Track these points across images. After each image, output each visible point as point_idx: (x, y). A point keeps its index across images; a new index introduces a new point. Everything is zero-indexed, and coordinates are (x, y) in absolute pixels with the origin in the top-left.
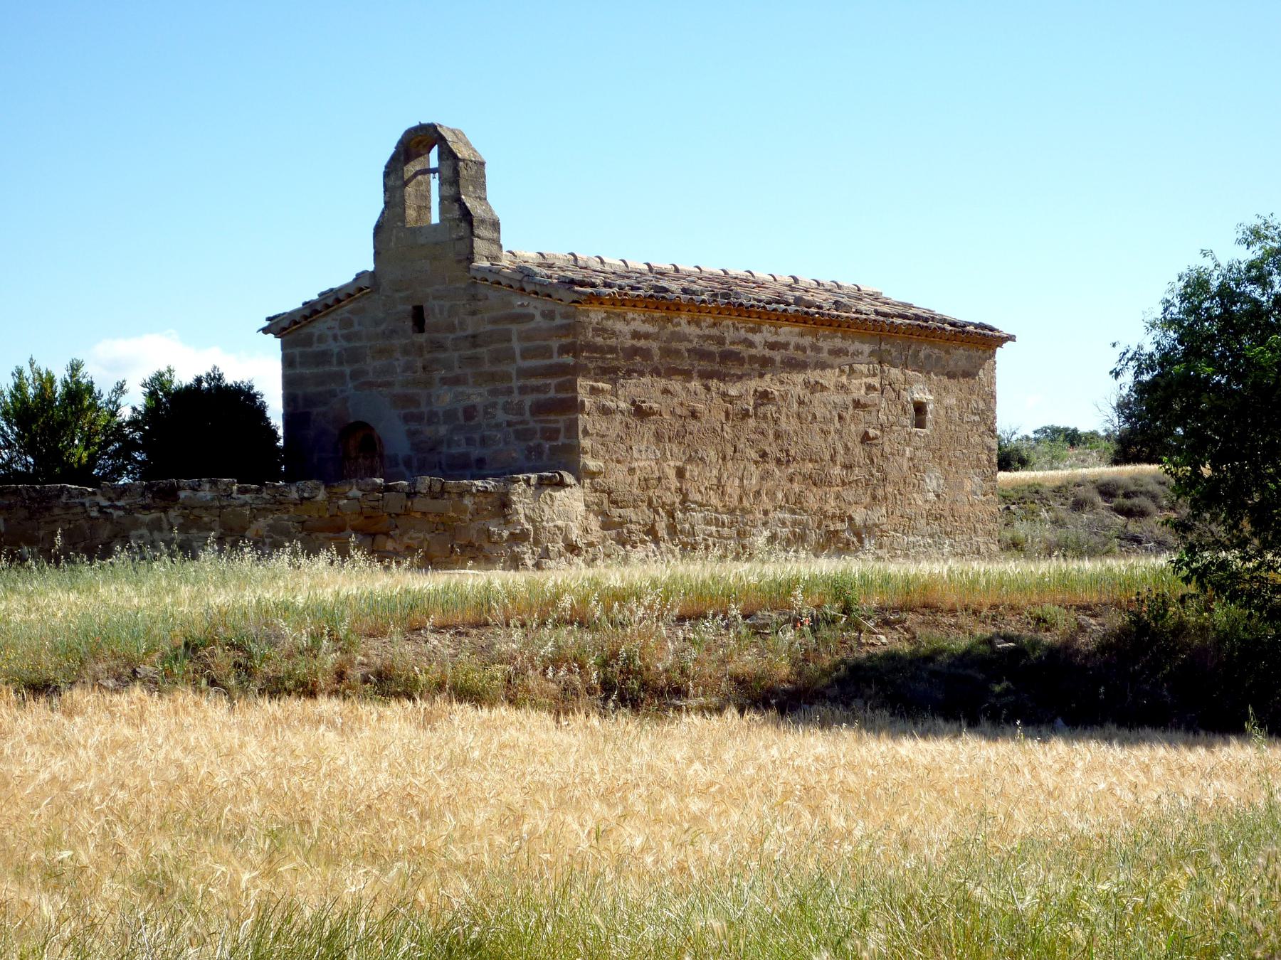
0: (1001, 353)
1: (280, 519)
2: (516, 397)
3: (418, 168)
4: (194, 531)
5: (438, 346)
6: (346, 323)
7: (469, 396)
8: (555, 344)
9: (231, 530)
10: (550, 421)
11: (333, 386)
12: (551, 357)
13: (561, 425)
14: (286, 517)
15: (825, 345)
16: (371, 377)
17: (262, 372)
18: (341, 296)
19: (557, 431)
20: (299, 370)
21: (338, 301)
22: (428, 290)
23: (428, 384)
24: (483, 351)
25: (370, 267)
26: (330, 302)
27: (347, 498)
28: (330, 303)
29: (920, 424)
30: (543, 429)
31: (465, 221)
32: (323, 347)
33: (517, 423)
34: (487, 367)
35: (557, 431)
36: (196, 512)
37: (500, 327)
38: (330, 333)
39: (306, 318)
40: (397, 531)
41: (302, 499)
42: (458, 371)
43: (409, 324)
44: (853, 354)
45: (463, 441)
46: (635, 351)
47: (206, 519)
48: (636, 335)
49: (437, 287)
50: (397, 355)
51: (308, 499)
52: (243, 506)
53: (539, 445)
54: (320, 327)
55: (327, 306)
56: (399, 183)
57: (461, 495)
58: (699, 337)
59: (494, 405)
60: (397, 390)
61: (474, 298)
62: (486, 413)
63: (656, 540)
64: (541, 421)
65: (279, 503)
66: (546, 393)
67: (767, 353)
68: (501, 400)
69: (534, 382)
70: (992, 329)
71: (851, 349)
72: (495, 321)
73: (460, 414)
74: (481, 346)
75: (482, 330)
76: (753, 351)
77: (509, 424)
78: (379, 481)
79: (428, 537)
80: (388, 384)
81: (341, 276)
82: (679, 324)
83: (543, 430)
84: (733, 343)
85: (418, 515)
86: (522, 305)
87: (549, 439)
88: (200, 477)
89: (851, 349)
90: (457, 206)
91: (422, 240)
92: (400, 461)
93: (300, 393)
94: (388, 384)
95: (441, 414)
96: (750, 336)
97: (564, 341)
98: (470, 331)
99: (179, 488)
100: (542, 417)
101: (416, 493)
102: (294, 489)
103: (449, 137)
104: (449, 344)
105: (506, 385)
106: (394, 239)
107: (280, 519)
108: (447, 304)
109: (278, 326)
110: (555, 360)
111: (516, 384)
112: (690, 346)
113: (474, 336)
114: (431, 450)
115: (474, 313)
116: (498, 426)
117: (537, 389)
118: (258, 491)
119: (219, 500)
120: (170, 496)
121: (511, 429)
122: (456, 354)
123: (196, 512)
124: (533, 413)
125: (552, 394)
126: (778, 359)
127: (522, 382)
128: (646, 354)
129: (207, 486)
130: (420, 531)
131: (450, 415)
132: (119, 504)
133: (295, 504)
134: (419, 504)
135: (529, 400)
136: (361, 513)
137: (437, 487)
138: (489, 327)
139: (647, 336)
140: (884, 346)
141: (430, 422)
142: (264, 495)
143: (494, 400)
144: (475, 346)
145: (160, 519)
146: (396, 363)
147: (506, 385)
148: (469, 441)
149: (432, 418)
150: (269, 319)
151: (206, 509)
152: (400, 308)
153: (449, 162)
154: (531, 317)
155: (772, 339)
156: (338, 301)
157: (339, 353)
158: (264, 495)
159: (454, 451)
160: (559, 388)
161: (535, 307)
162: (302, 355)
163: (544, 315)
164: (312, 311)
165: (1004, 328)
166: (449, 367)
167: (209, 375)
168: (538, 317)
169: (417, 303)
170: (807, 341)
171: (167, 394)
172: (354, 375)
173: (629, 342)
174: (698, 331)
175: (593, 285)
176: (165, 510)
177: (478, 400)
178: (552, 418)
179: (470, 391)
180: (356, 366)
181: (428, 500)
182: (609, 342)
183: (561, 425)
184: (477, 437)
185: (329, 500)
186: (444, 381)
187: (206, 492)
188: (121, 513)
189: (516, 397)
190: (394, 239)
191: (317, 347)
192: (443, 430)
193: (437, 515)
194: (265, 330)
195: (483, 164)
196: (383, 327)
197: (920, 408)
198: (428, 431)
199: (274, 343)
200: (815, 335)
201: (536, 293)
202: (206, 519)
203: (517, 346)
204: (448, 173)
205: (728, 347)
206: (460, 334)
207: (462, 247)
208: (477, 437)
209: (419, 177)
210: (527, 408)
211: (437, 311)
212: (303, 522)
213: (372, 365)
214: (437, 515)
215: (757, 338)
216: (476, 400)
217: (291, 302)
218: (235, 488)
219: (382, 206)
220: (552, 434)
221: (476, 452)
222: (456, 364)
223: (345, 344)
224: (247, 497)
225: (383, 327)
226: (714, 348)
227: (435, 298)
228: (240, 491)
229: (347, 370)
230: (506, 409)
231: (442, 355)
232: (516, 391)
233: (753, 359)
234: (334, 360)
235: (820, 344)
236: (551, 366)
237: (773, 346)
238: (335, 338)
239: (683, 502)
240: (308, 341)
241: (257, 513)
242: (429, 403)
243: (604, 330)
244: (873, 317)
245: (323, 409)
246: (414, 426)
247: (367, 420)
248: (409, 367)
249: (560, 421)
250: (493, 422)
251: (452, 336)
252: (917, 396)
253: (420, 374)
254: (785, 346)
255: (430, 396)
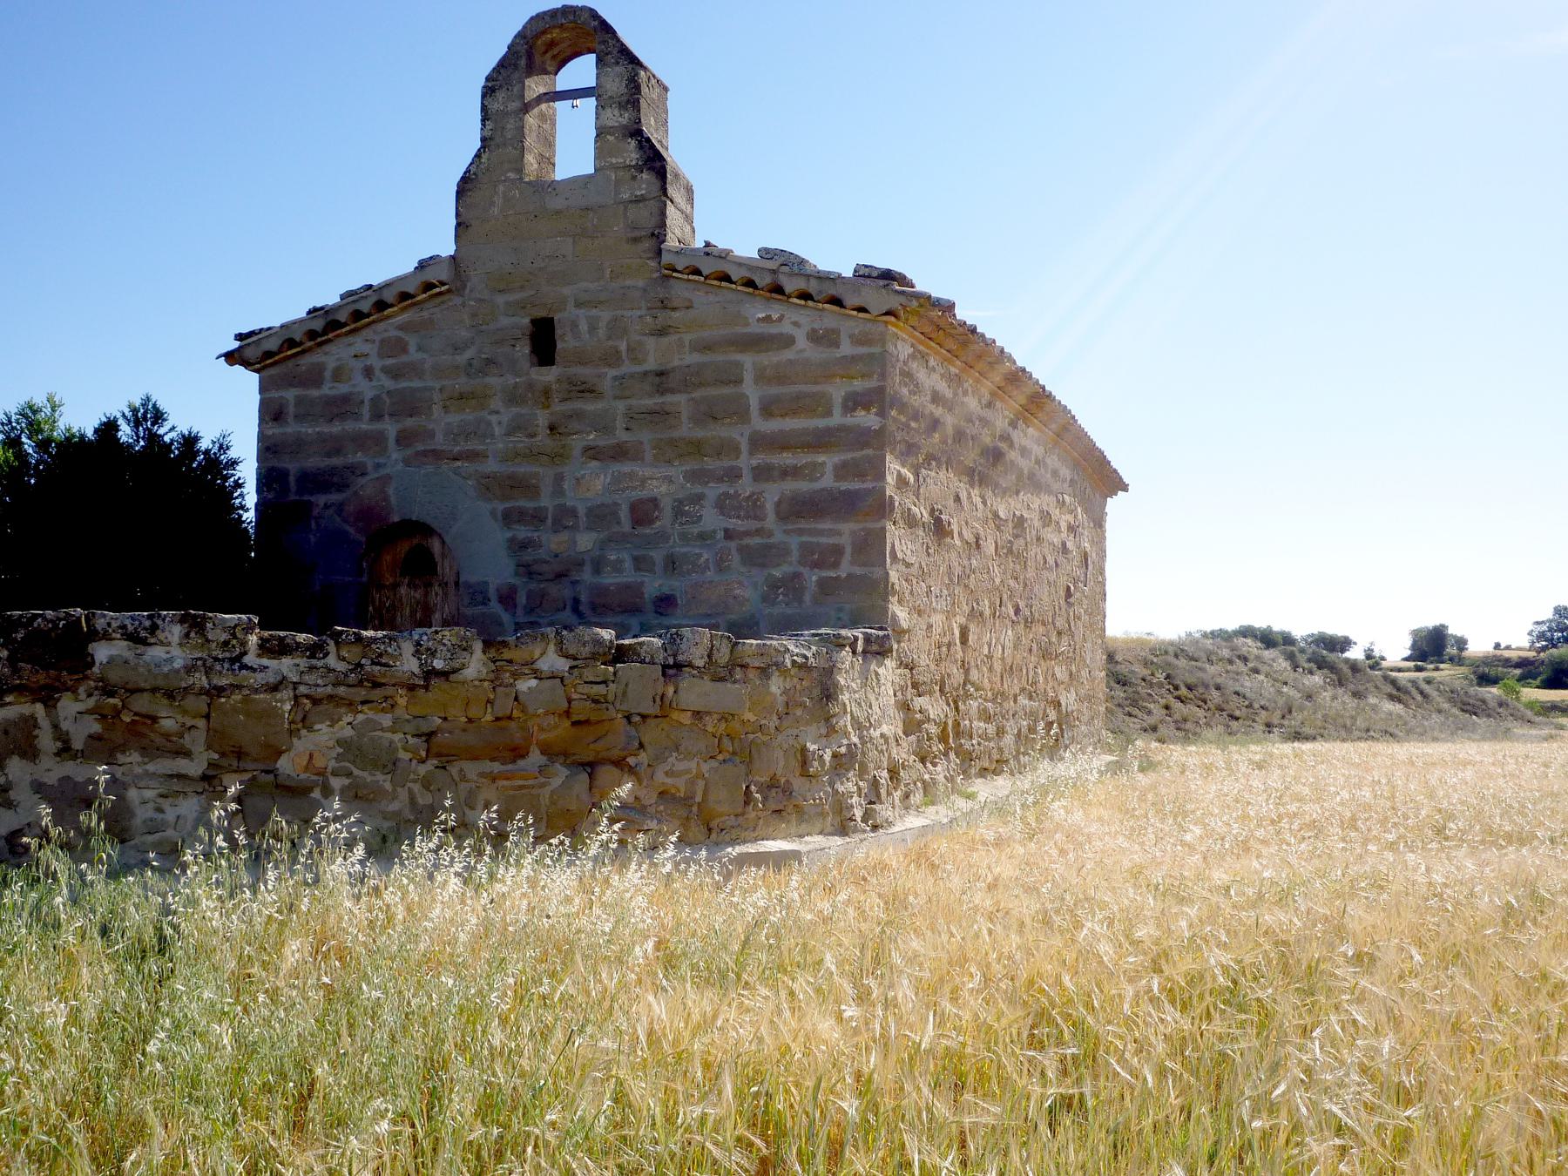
1: (372, 725)
2: (746, 486)
3: (542, 90)
4: (135, 757)
5: (587, 390)
6: (394, 347)
7: (643, 481)
8: (837, 391)
9: (240, 754)
10: (821, 533)
11: (360, 457)
12: (828, 413)
13: (845, 540)
14: (386, 720)
16: (440, 443)
17: (223, 415)
18: (389, 296)
19: (838, 551)
20: (291, 428)
21: (381, 305)
22: (566, 291)
23: (557, 457)
24: (679, 401)
25: (447, 248)
26: (365, 306)
27: (537, 674)
28: (364, 310)
30: (803, 546)
32: (343, 389)
33: (747, 534)
34: (685, 429)
35: (838, 551)
36: (142, 703)
37: (719, 358)
38: (359, 365)
39: (312, 334)
40: (643, 757)
41: (430, 674)
42: (623, 436)
43: (524, 349)
45: (628, 564)
47: (168, 724)
49: (584, 285)
50: (496, 403)
51: (445, 675)
52: (274, 688)
54: (336, 354)
55: (357, 315)
56: (514, 105)
57: (764, 672)
59: (698, 499)
60: (491, 466)
61: (664, 305)
62: (678, 512)
64: (801, 532)
65: (369, 683)
66: (813, 479)
68: (713, 491)
69: (787, 459)
72: (706, 347)
73: (624, 514)
74: (673, 391)
75: (676, 363)
78: (607, 634)
79: (705, 767)
80: (472, 456)
81: (389, 263)
83: (806, 549)
85: (686, 719)
86: (768, 319)
87: (817, 565)
88: (153, 603)
90: (633, 143)
91: (556, 203)
93: (292, 466)
94: (472, 456)
95: (582, 511)
97: (859, 385)
98: (651, 364)
99: (94, 635)
100: (803, 524)
101: (678, 666)
102: (408, 648)
104: (606, 385)
105: (726, 463)
106: (498, 200)
107: (372, 725)
108: (605, 315)
109: (250, 352)
110: (837, 419)
111: (746, 461)
113: (661, 374)
114: (560, 576)
115: (662, 332)
118: (315, 650)
119: (208, 671)
121: (733, 545)
122: (621, 406)
123: (142, 703)
124: (783, 517)
125: (827, 481)
127: (759, 459)
129: (177, 631)
130: (689, 756)
131: (600, 516)
133: (412, 688)
134: (693, 692)
135: (772, 493)
136: (567, 713)
137: (723, 655)
141: (558, 526)
142: (332, 661)
143: (698, 489)
144: (662, 390)
145: (30, 722)
146: (494, 418)
147: (726, 463)
148: (640, 563)
149: (564, 518)
150: (239, 337)
151: (170, 695)
152: (505, 321)
153: (618, 69)
154: (789, 341)
156: (381, 305)
157: (376, 401)
158: (332, 661)
159: (609, 579)
160: (842, 471)
161: (795, 321)
162: (299, 401)
163: (814, 337)
164: (326, 325)
166: (606, 429)
167: (135, 411)
168: (802, 342)
169: (542, 314)
171: (43, 445)
172: (404, 439)
177: (663, 489)
178: (826, 525)
179: (648, 472)
180: (409, 422)
181: (707, 685)
183: (845, 540)
184: (657, 555)
185: (496, 682)
186: (592, 453)
187: (172, 648)
189: (746, 486)
190: (498, 200)
191: (328, 389)
192: (586, 541)
193: (723, 718)
194: (231, 357)
196: (469, 354)
198: (553, 542)
199: (247, 383)
201: (805, 296)
202: (168, 724)
203: (753, 393)
206: (627, 368)
207: (643, 216)
208: (657, 555)
209: (543, 106)
210: (770, 507)
211: (583, 327)
212: (429, 736)
213: (441, 422)
214: (723, 718)
216: (658, 489)
217: (282, 306)
218: (253, 639)
219: (479, 144)
220: (828, 557)
221: (653, 585)
222: (620, 423)
223: (389, 384)
224: (286, 666)
225: (469, 354)
227: (578, 305)
228: (265, 648)
229: (390, 428)
230: (721, 505)
231: (590, 406)
234: (366, 411)
236: (828, 431)
238: (368, 372)
240: (314, 378)
241: (310, 709)
242: (558, 491)
245: (335, 497)
246: (522, 532)
247: (428, 520)
249: (846, 531)
250: (695, 530)
251: (612, 372)
253: (543, 439)
255: (559, 478)
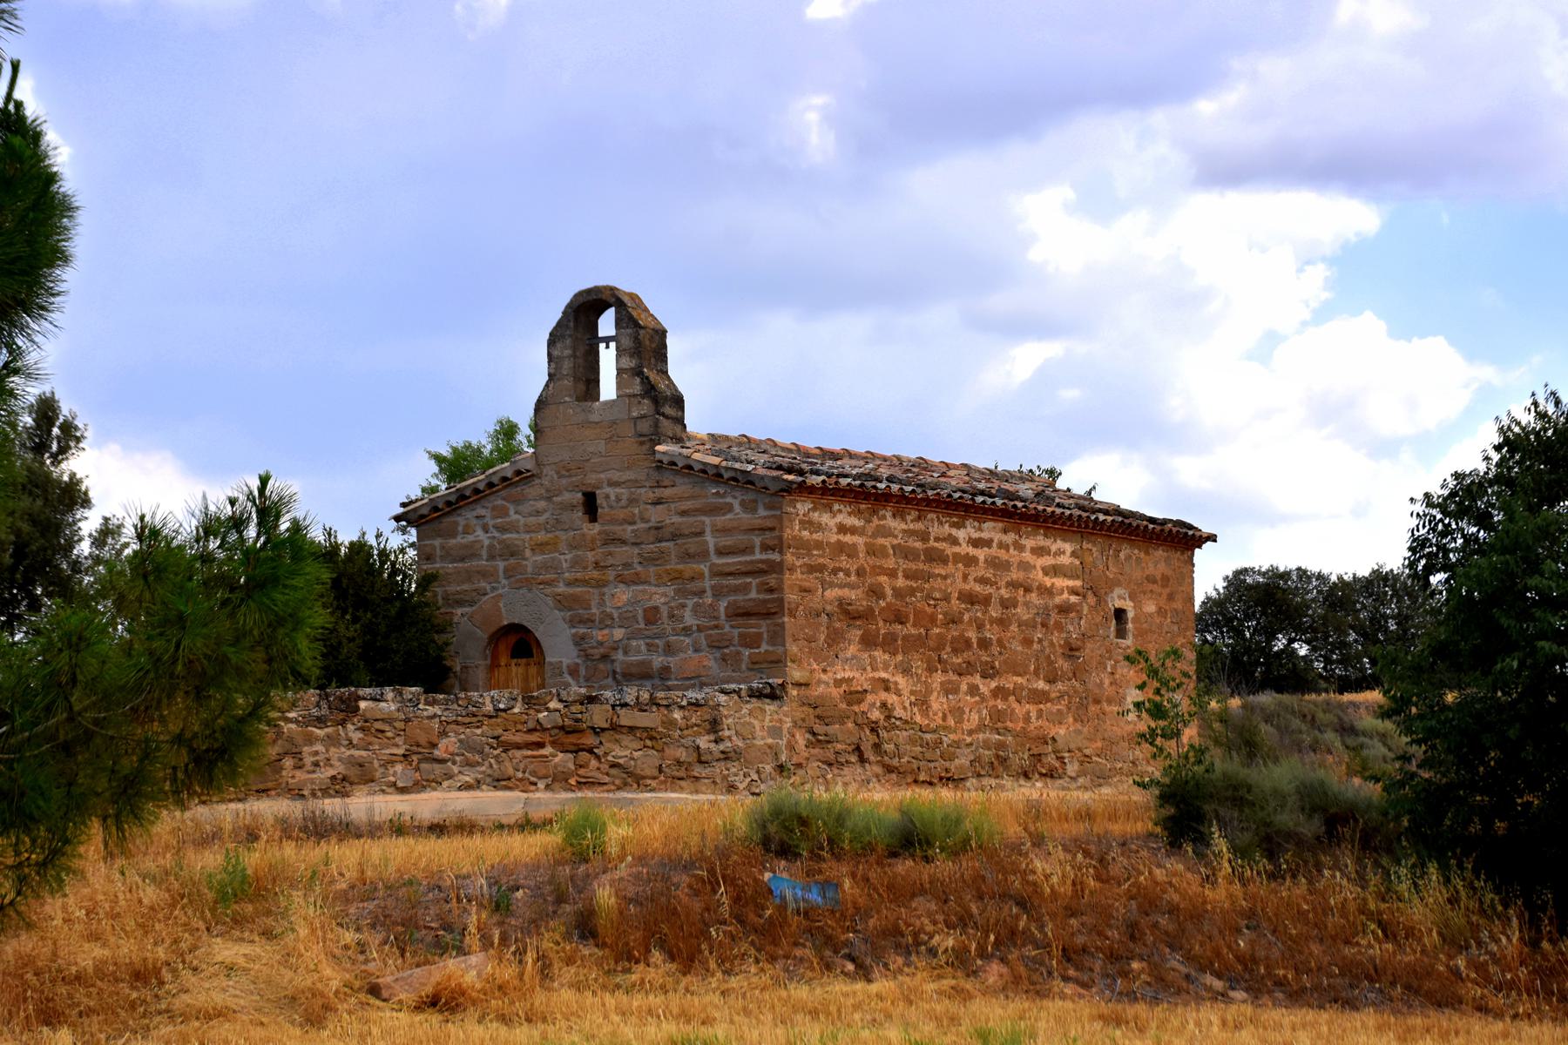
0: (1199, 555)
15: (1029, 543)
27: (548, 709)
29: (1121, 633)
31: (658, 400)
34: (674, 565)
44: (1055, 554)
45: (643, 648)
46: (841, 548)
48: (842, 529)
53: (738, 653)
58: (905, 531)
62: (671, 616)
63: (862, 760)
67: (971, 551)
70: (1191, 527)
71: (1054, 548)
76: (956, 549)
77: (700, 629)
82: (884, 517)
84: (937, 539)
86: (717, 493)
89: (1054, 548)
90: (638, 380)
92: (565, 669)
96: (954, 531)
103: (626, 299)
112: (895, 542)
116: (687, 631)
117: (736, 590)
120: (349, 708)
126: (982, 558)
128: (851, 551)
131: (626, 620)
132: (292, 715)
138: (677, 519)
139: (853, 530)
140: (1085, 546)
155: (976, 535)
165: (1206, 528)
170: (1010, 538)
173: (834, 538)
174: (904, 526)
175: (801, 473)
176: (343, 723)
182: (815, 536)
188: (293, 726)
192: (619, 633)
195: (664, 332)
197: (1120, 614)
198: (599, 635)
200: (1018, 532)
203: (710, 540)
204: (627, 342)
205: (932, 543)
215: (961, 534)
216: (658, 600)
221: (658, 661)
226: (918, 545)
232: (709, 593)
233: (957, 558)
235: (1023, 542)
237: (976, 543)
239: (888, 717)
242: (602, 603)
243: (810, 523)
244: (1076, 512)
248: (575, 563)
252: (1118, 604)
254: (988, 543)
